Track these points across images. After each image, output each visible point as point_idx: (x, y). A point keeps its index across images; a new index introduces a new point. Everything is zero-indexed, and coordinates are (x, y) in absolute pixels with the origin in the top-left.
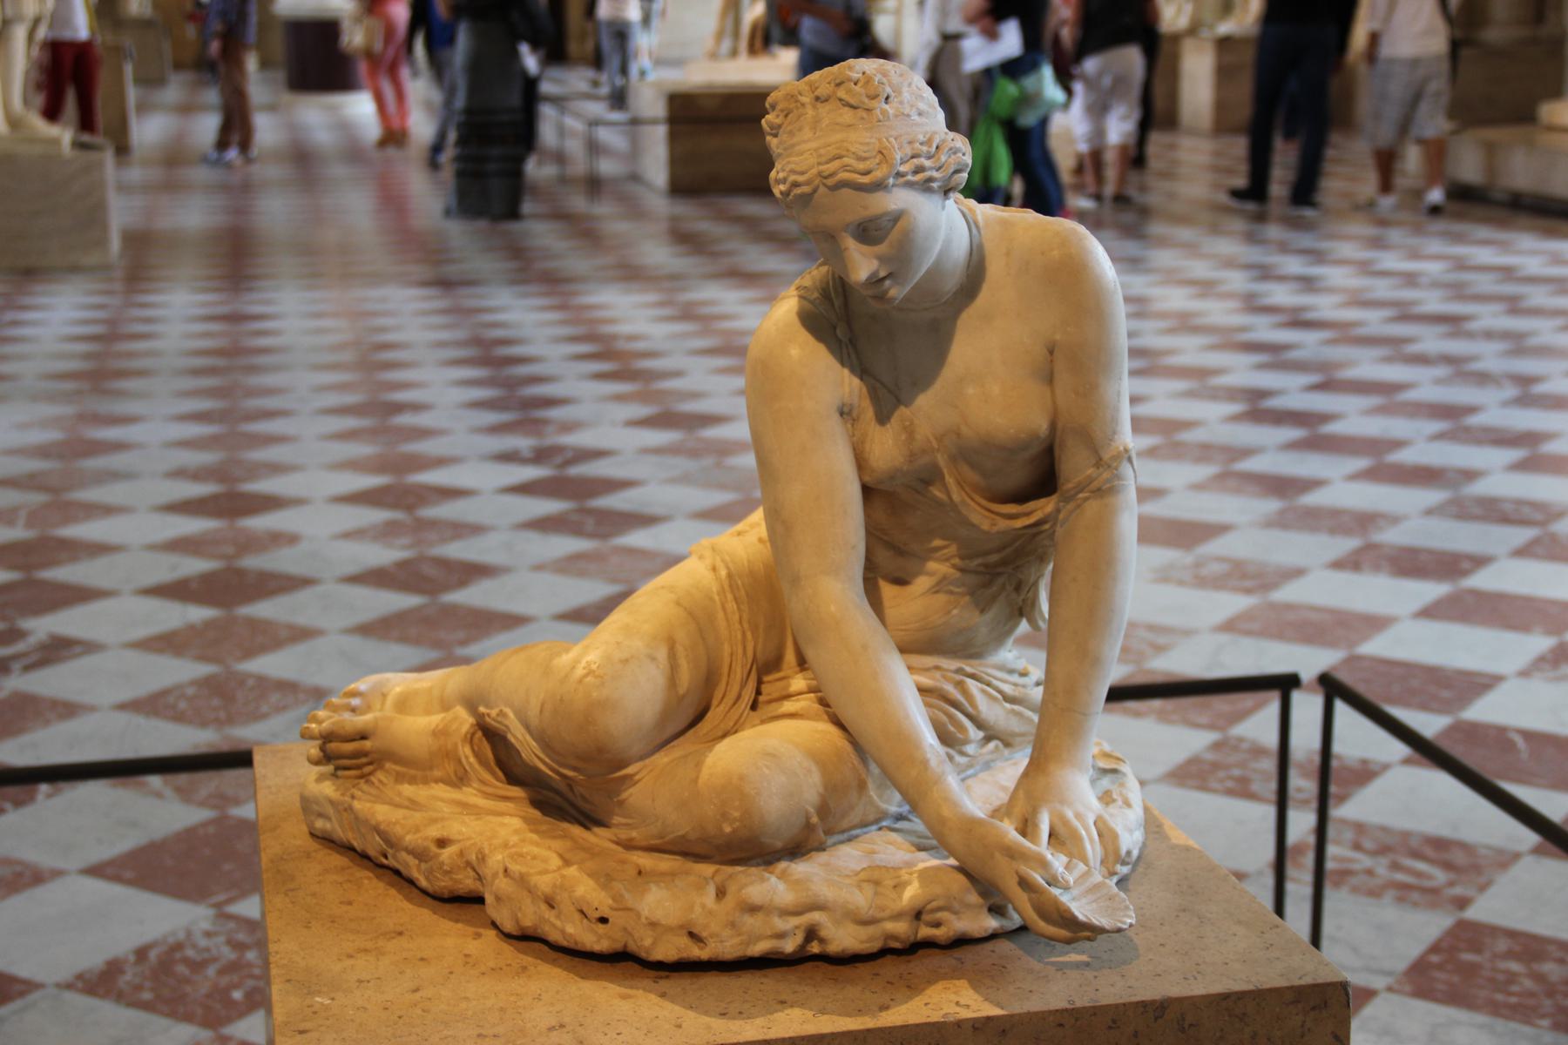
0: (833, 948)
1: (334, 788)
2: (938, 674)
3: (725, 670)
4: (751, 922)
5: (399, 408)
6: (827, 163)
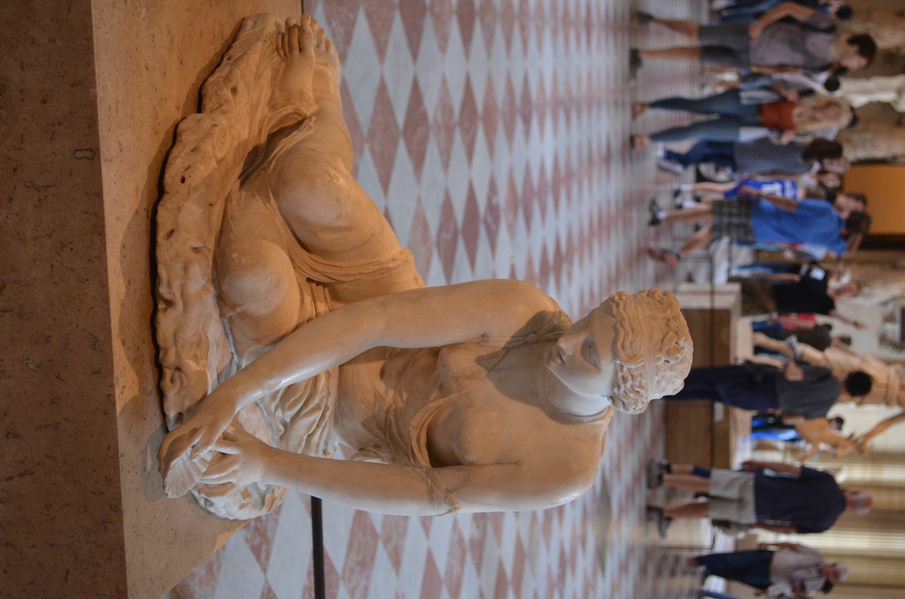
0: (161, 316)
1: (271, 32)
2: (325, 394)
3: (331, 263)
4: (179, 266)
5: (527, 122)
6: (630, 324)
